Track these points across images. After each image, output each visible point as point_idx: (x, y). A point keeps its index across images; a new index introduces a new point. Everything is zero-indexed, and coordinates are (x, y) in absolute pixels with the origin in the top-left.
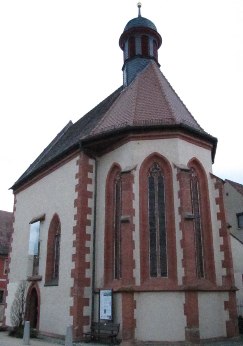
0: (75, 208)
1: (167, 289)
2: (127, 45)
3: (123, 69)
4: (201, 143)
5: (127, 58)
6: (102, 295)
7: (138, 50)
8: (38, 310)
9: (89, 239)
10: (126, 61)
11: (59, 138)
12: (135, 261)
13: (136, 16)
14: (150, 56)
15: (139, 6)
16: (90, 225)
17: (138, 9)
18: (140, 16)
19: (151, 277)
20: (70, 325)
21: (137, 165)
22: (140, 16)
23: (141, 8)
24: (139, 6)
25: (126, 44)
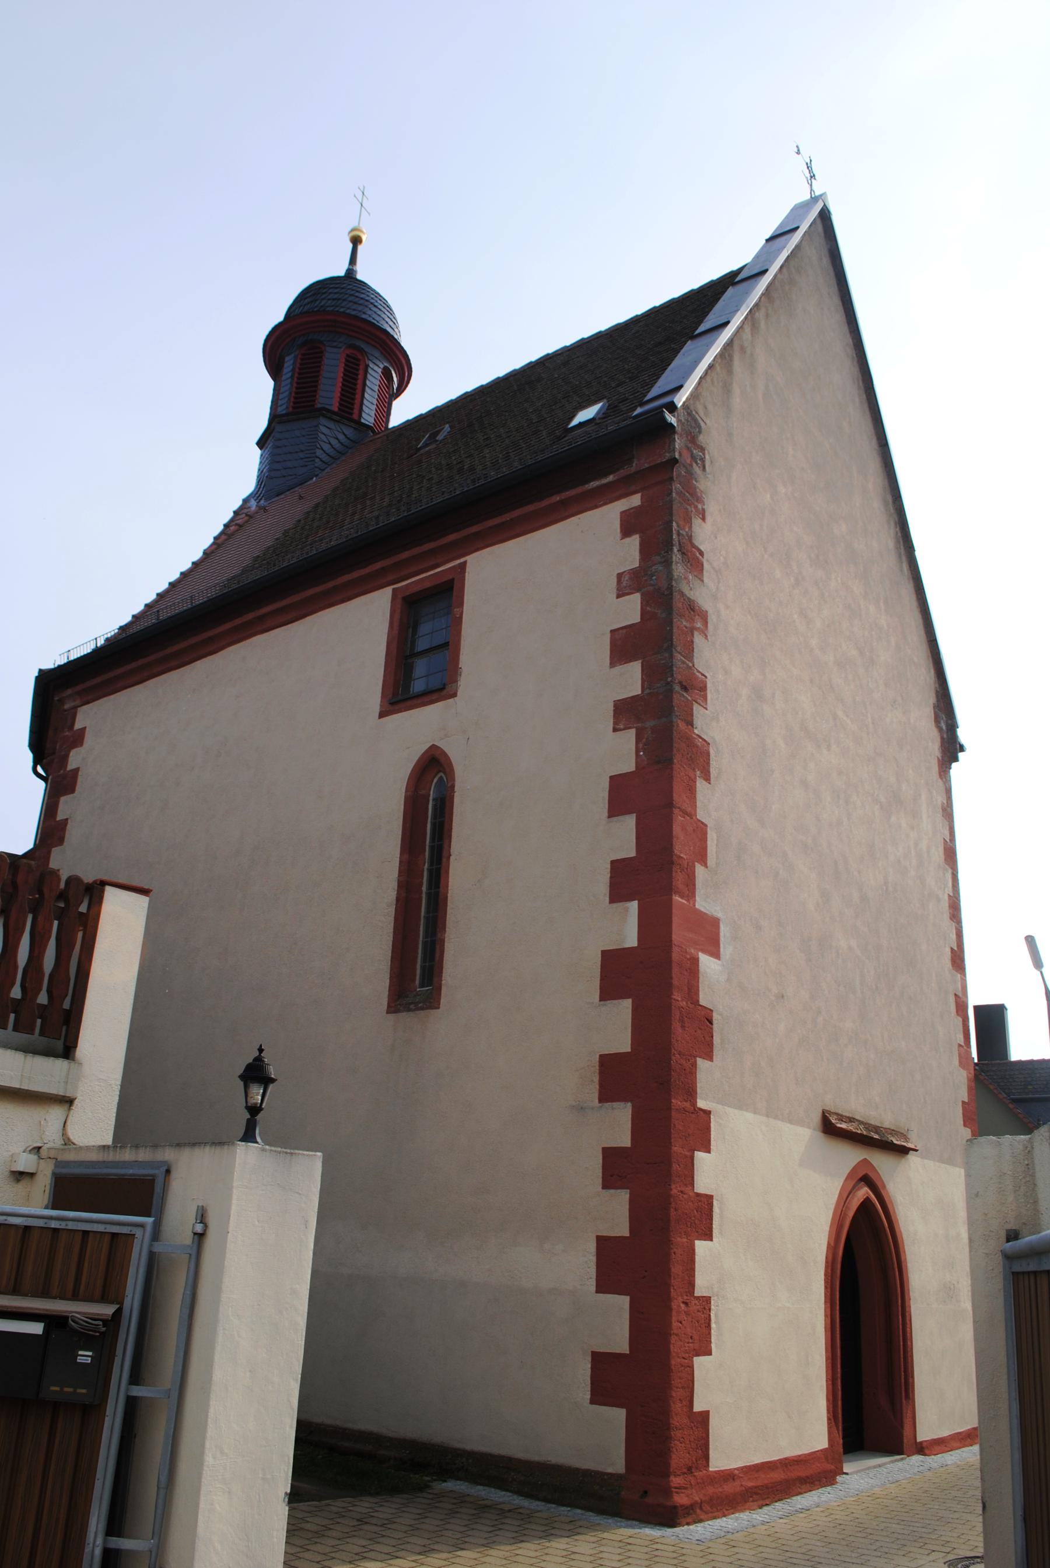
0: (627, 540)
2: (288, 364)
3: (261, 443)
4: (211, 639)
5: (281, 410)
6: (949, 1291)
7: (329, 394)
8: (106, 636)
10: (275, 418)
11: (142, 1178)
13: (341, 272)
14: (363, 421)
15: (356, 241)
17: (350, 246)
18: (350, 273)
20: (666, 1531)
21: (703, 557)
22: (350, 273)
23: (360, 248)
24: (356, 241)
25: (287, 359)
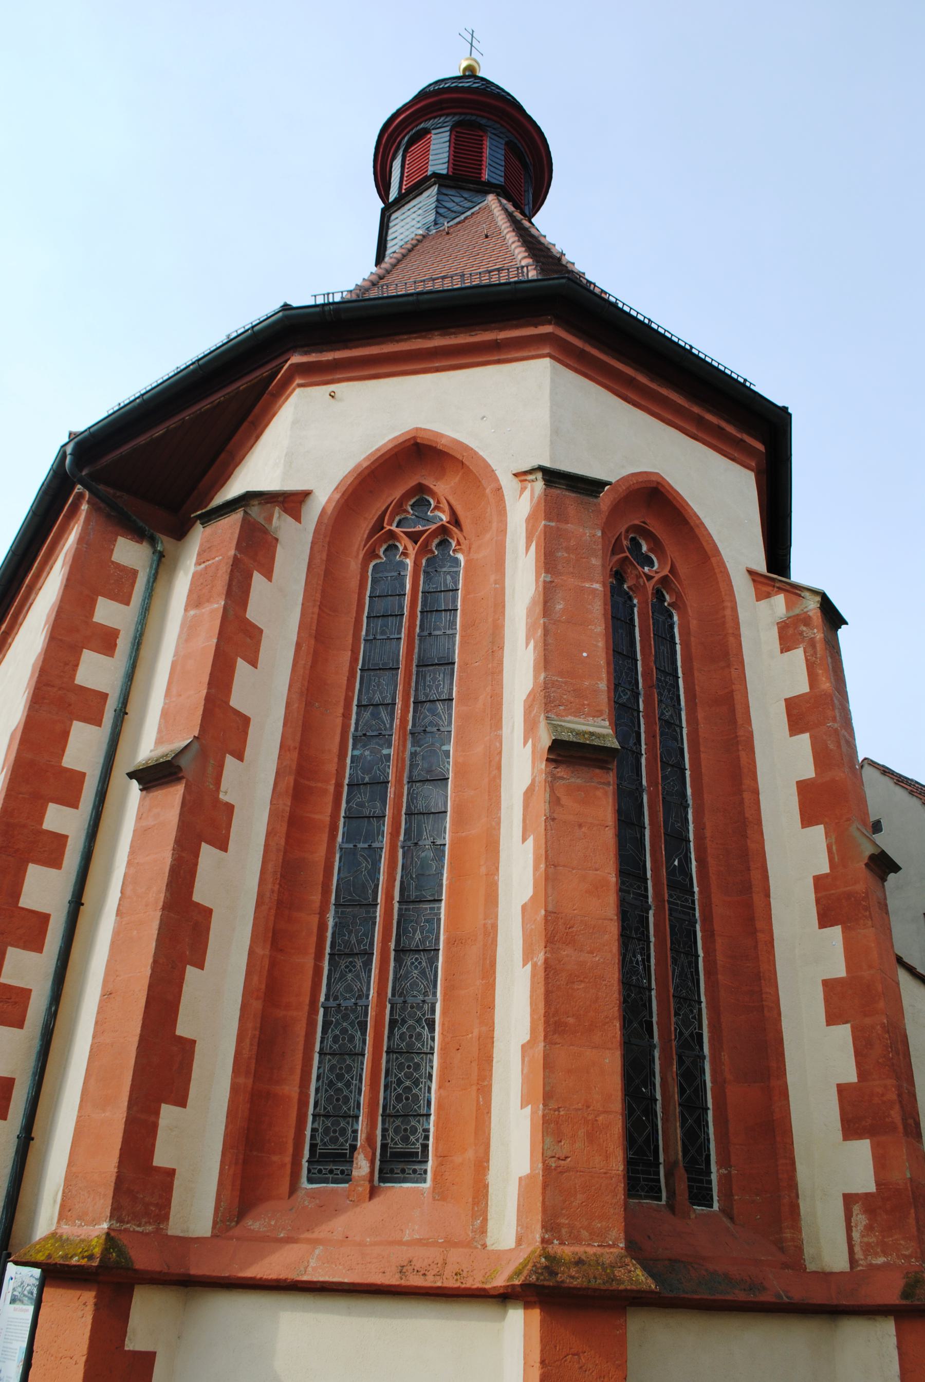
1: (391, 1279)
9: (35, 943)
12: (187, 1047)
16: (55, 861)
19: (310, 1180)
